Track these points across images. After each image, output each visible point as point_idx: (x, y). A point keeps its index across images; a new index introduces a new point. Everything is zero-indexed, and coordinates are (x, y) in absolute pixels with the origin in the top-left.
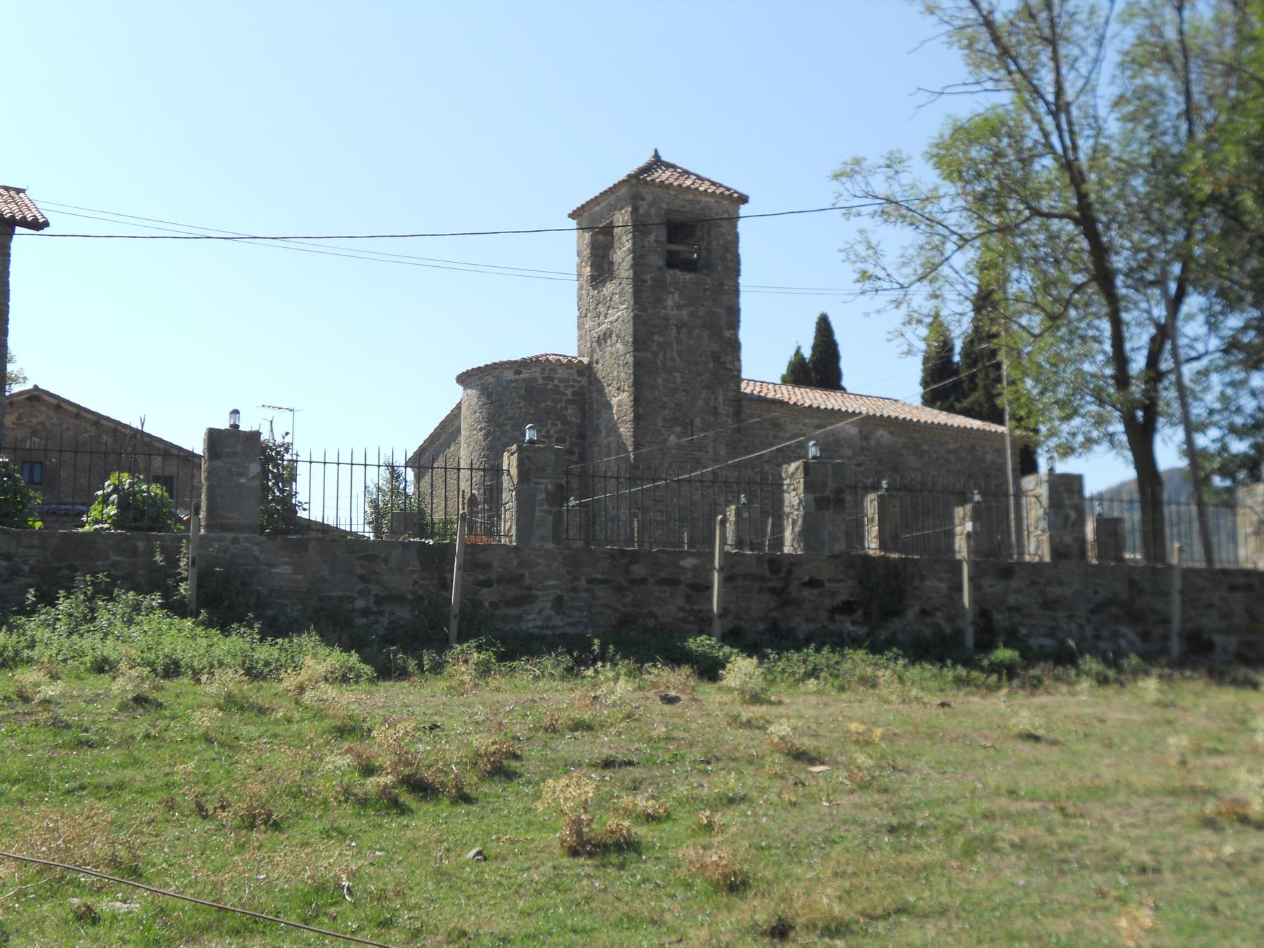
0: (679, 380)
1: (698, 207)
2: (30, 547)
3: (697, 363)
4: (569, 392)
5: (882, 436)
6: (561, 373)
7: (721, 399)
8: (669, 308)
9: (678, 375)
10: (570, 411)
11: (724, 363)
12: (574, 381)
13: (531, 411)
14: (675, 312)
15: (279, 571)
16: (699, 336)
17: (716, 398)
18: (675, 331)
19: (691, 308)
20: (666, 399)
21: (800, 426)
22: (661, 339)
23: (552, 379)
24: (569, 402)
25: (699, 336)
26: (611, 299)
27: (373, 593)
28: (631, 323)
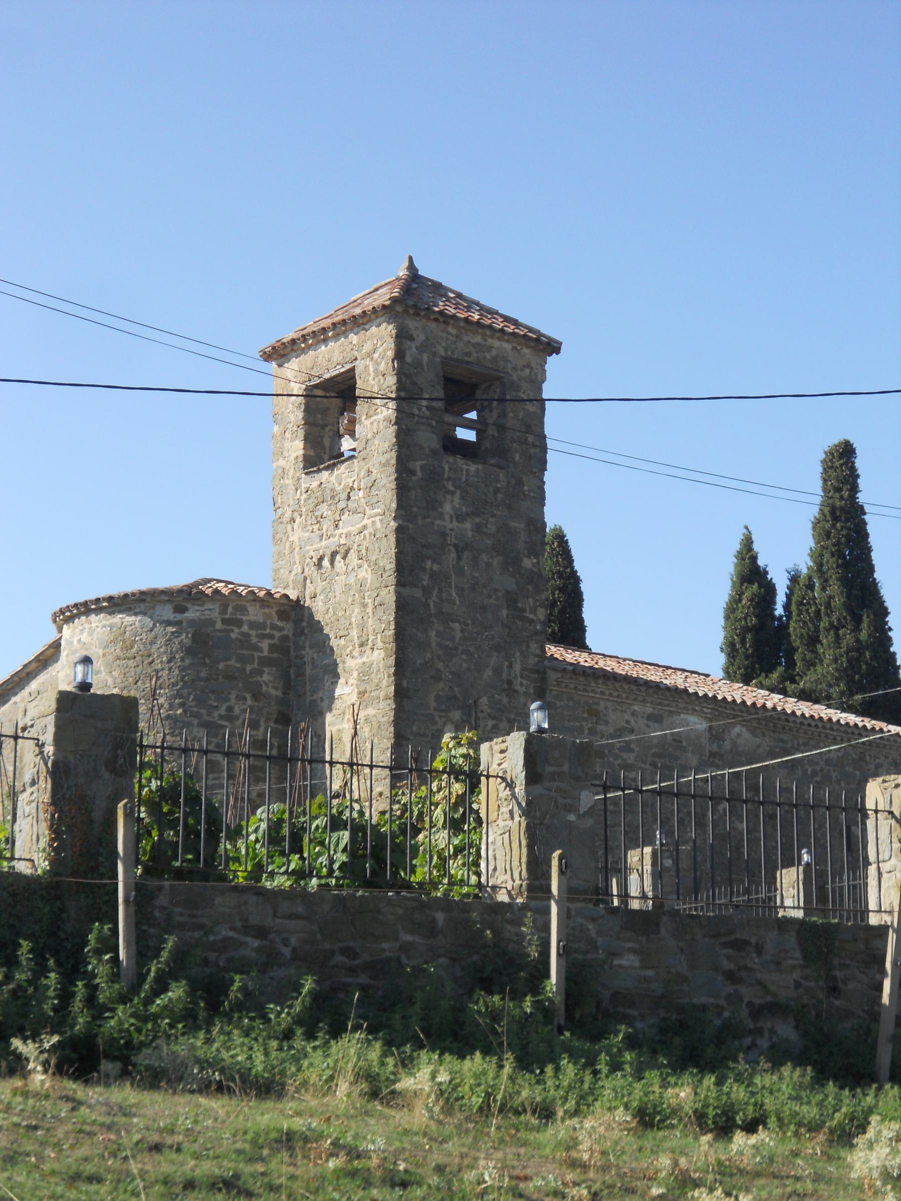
0: (458, 635)
1: (488, 356)
2: (292, 917)
3: (484, 608)
4: (265, 645)
5: (739, 735)
6: (254, 614)
7: (517, 667)
8: (447, 517)
9: (456, 626)
10: (266, 677)
11: (523, 610)
12: (274, 627)
13: (203, 674)
14: (455, 524)
15: (624, 962)
16: (488, 565)
17: (510, 666)
18: (453, 555)
19: (477, 520)
20: (440, 665)
21: (627, 717)
22: (436, 567)
23: (239, 623)
24: (264, 661)
25: (488, 565)
26: (349, 498)
27: (746, 1000)
28: (392, 539)
